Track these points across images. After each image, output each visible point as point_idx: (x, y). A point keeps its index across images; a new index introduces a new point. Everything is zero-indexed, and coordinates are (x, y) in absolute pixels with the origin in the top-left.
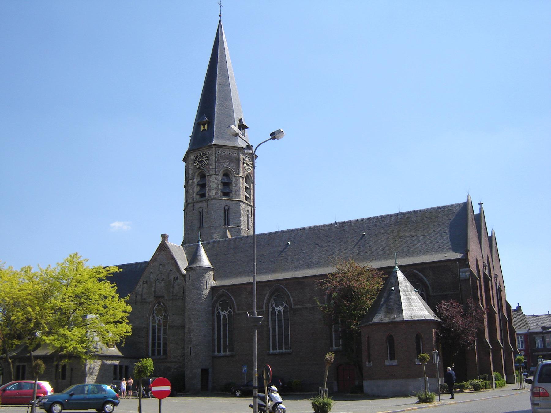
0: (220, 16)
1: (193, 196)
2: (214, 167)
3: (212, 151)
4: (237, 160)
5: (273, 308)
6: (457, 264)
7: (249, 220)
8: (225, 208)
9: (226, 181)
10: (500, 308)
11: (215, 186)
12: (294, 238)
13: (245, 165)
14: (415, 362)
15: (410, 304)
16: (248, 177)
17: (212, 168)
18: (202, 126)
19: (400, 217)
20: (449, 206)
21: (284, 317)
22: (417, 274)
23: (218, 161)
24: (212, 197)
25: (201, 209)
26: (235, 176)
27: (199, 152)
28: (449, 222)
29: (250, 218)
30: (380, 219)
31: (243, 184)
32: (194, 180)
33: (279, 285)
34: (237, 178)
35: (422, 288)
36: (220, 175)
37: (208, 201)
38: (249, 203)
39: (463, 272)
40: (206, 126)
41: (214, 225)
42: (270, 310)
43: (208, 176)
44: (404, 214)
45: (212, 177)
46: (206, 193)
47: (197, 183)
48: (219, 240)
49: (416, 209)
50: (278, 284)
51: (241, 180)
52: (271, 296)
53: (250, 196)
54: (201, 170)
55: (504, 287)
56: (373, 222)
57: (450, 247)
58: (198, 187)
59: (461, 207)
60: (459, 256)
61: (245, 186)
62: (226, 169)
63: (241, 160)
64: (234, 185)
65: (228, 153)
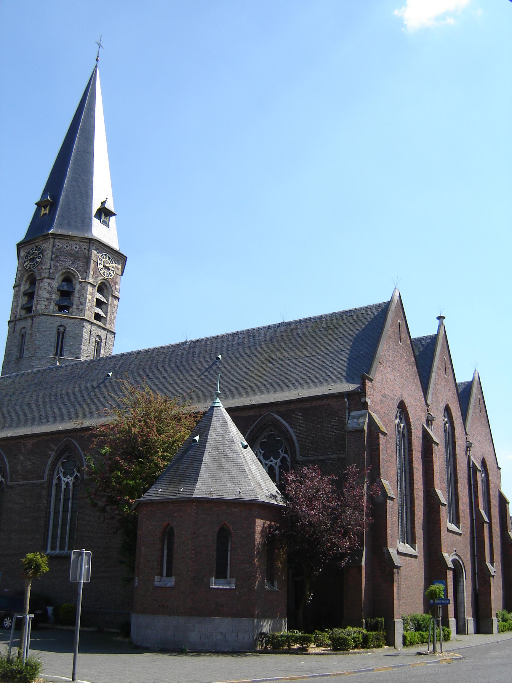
0: (97, 60)
1: (16, 311)
2: (49, 267)
3: (48, 244)
4: (85, 259)
5: (59, 479)
6: (345, 403)
7: (100, 351)
8: (59, 329)
9: (65, 288)
10: (473, 500)
11: (46, 295)
12: (120, 367)
13: (100, 267)
14: (209, 584)
15: (220, 469)
16: (106, 286)
17: (45, 268)
18: (43, 209)
19: (281, 329)
20: (361, 309)
21: (73, 495)
22: (279, 421)
23: (56, 258)
24: (40, 312)
25: (24, 331)
26: (80, 282)
27: (31, 246)
28: (355, 333)
29: (102, 348)
30: (250, 334)
31: (91, 294)
32: (20, 287)
33: (70, 440)
34: (83, 284)
35: (286, 449)
36: (56, 279)
37: (34, 318)
38: (104, 326)
39: (354, 417)
40: (48, 209)
41: (37, 354)
42: (55, 482)
43: (38, 280)
44: (289, 324)
45: (44, 282)
46: (33, 305)
47: (24, 292)
48: (24, 372)
49: (308, 316)
50: (69, 438)
51: (90, 288)
52: (57, 459)
53: (106, 315)
54: (31, 273)
55: (496, 469)
56: (239, 338)
57: (344, 373)
58: (25, 298)
59: (381, 308)
60: (352, 387)
61: (97, 299)
62: (66, 270)
63: (93, 257)
64: (76, 295)
65: (74, 247)
